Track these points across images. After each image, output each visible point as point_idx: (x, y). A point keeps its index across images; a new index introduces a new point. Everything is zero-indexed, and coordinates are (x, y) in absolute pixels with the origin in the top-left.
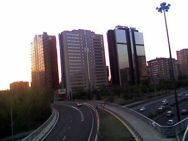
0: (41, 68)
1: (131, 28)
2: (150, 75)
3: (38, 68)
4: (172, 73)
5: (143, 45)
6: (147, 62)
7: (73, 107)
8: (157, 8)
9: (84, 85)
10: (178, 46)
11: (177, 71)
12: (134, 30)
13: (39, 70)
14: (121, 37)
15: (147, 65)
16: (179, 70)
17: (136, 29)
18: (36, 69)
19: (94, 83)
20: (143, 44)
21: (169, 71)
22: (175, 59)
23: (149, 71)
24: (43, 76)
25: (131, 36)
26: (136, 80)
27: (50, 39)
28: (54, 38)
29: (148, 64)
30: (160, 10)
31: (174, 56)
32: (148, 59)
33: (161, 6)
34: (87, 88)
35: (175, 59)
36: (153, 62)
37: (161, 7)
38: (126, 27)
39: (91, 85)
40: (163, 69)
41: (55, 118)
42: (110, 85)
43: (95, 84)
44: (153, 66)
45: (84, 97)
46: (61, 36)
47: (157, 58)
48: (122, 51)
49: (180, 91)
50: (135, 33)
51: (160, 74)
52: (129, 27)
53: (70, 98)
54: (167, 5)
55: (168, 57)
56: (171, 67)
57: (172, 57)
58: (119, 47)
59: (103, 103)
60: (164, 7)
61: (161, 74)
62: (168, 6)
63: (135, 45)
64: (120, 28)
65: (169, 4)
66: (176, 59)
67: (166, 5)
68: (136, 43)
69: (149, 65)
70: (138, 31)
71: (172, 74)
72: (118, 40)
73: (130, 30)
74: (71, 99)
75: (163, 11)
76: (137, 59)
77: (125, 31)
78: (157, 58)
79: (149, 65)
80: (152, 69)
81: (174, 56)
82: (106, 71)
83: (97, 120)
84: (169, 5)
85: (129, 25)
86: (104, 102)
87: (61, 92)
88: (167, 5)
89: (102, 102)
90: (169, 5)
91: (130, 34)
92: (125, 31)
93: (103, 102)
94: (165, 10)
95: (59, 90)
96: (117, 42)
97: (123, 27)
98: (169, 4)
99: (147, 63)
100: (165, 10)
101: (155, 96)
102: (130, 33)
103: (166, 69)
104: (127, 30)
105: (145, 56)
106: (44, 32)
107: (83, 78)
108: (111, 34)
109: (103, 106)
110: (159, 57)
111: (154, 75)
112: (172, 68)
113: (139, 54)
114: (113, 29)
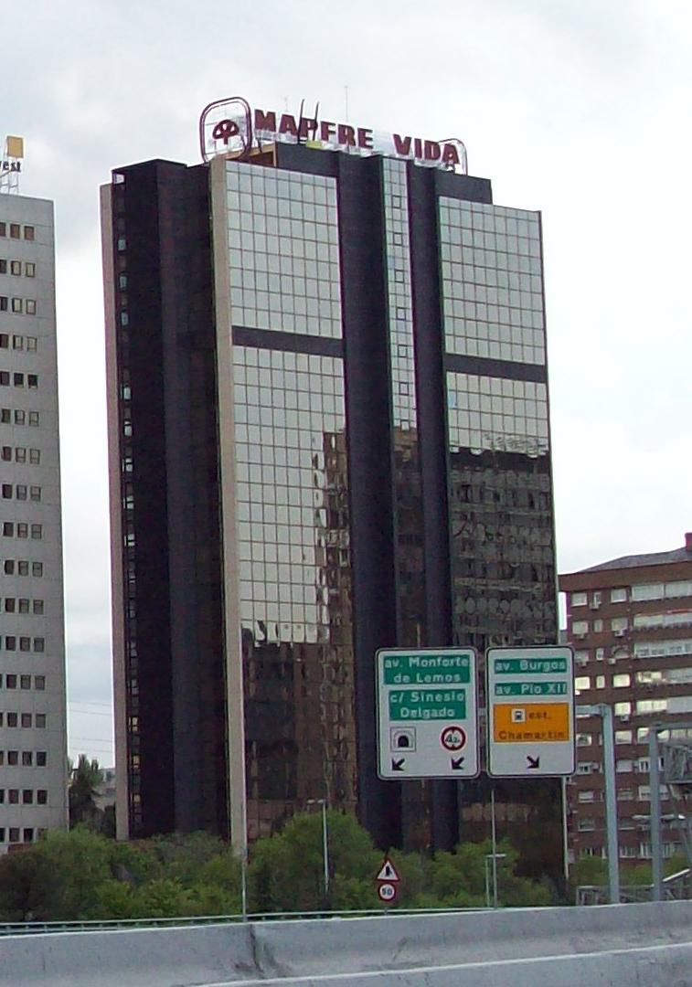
1: (402, 145)
4: (507, 667)
5: (538, 374)
6: (576, 583)
12: (438, 180)
14: (275, 257)
17: (474, 165)
25: (398, 256)
36: (641, 594)
38: (346, 133)
44: (640, 651)
48: (278, 428)
50: (451, 211)
52: (382, 143)
58: (244, 376)
64: (289, 147)
68: (451, 346)
69: (581, 628)
70: (479, 190)
72: (244, 295)
73: (395, 187)
77: (333, 181)
79: (581, 628)
80: (622, 681)
83: (289, 983)
85: (389, 115)
92: (333, 181)
93: (388, 872)
97: (314, 140)
102: (397, 220)
104: (357, 177)
108: (160, 219)
114: (193, 159)
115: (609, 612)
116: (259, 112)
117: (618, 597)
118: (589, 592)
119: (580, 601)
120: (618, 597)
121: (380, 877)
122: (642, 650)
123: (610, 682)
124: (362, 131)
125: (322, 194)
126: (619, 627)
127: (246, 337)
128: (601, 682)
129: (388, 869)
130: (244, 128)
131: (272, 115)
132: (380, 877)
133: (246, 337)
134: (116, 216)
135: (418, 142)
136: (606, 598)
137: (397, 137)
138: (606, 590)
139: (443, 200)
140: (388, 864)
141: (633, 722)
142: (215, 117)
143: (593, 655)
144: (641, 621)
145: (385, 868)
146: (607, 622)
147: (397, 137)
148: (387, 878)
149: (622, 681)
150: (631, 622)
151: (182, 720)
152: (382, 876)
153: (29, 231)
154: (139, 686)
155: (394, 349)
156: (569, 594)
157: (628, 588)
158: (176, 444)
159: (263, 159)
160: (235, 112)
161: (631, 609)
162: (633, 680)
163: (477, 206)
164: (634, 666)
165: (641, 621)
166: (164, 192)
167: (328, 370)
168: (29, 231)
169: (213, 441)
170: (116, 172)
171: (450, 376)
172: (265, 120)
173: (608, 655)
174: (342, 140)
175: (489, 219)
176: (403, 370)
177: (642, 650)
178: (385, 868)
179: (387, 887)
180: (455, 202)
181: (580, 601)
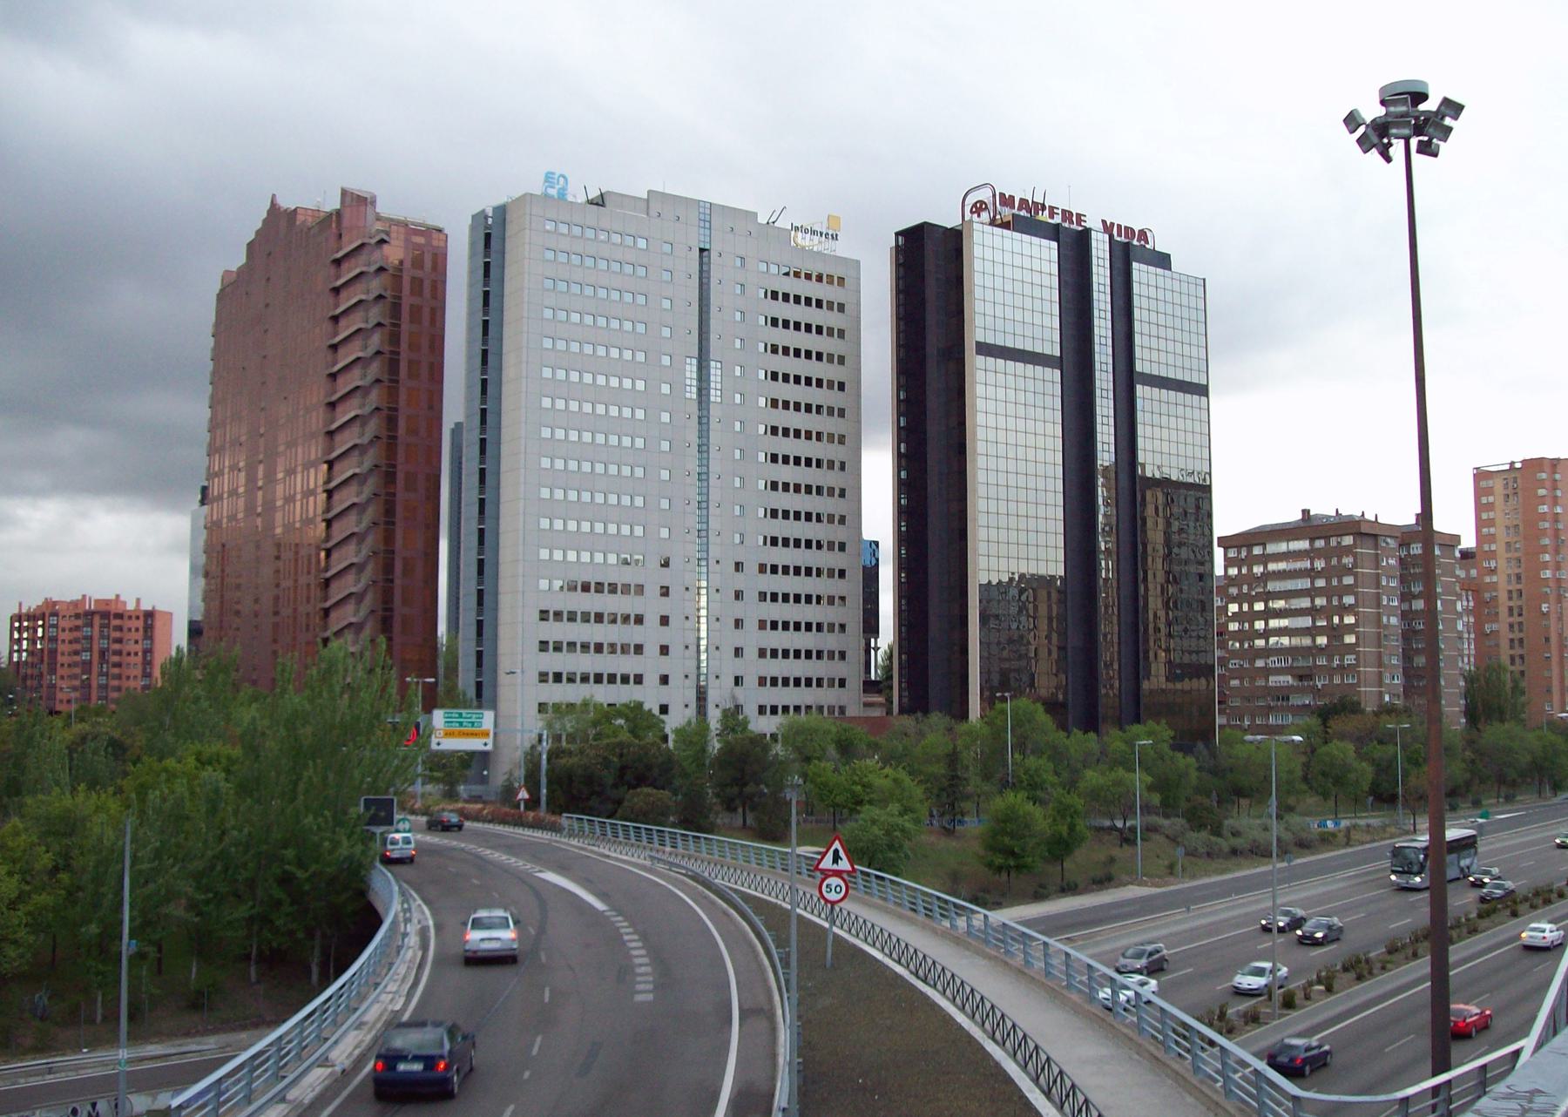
0: (290, 499)
1: (1107, 228)
2: (1235, 683)
3: (270, 507)
5: (1202, 390)
6: (1226, 542)
7: (551, 877)
8: (1352, 121)
9: (649, 697)
10: (1486, 431)
11: (1469, 648)
12: (1130, 251)
13: (270, 526)
14: (1011, 287)
15: (1219, 570)
16: (1481, 636)
18: (250, 509)
19: (738, 681)
20: (1195, 379)
21: (1394, 621)
22: (1456, 539)
23: (1234, 626)
24: (303, 580)
26: (1111, 686)
27: (394, 253)
28: (427, 249)
29: (1229, 562)
30: (1376, 137)
31: (1456, 517)
32: (1228, 519)
33: (1383, 103)
34: (672, 722)
35: (1456, 539)
36: (1272, 548)
37: (1381, 111)
38: (1067, 215)
39: (713, 696)
40: (1349, 620)
41: (411, 950)
42: (877, 713)
43: (751, 697)
44: (1271, 586)
45: (644, 795)
46: (491, 236)
47: (1305, 512)
48: (1013, 431)
49: (1313, 569)
50: (1141, 272)
51: (1322, 661)
53: (523, 794)
54: (1430, 105)
55: (1403, 513)
56: (1419, 605)
57: (1440, 524)
59: (838, 873)
60: (1409, 122)
61: (1330, 660)
62: (1439, 115)
63: (1127, 379)
64: (1024, 218)
65: (1446, 102)
66: (1468, 541)
67: (1422, 107)
68: (1138, 368)
69: (1233, 571)
70: (1163, 261)
71: (1421, 677)
73: (1100, 248)
74: (533, 803)
75: (1397, 149)
76: (1134, 517)
77: (1054, 245)
78: (1305, 512)
79: (1233, 571)
80: (1259, 606)
81: (1456, 517)
82: (852, 587)
84: (1453, 108)
86: (844, 864)
87: (448, 734)
88: (1430, 105)
89: (827, 863)
90: (1453, 108)
91: (1098, 270)
93: (836, 858)
94: (1414, 142)
95: (439, 717)
96: (980, 336)
97: (1044, 216)
98: (1446, 102)
99: (1219, 553)
100: (1414, 142)
101: (1266, 854)
103: (1378, 597)
104: (1074, 246)
105: (1207, 489)
106: (344, 193)
107: (651, 635)
109: (833, 896)
110: (1323, 508)
111: (1274, 680)
112: (1431, 614)
113: (1159, 454)
114: (950, 220)
115: (1251, 560)
116: (1002, 195)
117: (1257, 551)
118: (1239, 547)
119: (1232, 554)
120: (1257, 551)
121: (822, 866)
122: (1272, 586)
123: (1251, 607)
124: (1079, 216)
125: (1046, 253)
126: (1258, 570)
127: (985, 349)
128: (1245, 607)
129: (836, 851)
130: (991, 207)
131: (1012, 198)
132: (822, 866)
133: (985, 349)
134: (898, 265)
135: (1119, 226)
136: (1250, 551)
137: (1104, 222)
138: (1250, 547)
139: (1135, 265)
140: (837, 845)
141: (1267, 634)
142: (971, 200)
143: (1240, 589)
144: (1272, 567)
145: (831, 852)
146: (1252, 679)
147: (1104, 222)
148: (835, 867)
149: (1259, 606)
150: (1265, 567)
151: (936, 627)
152: (827, 863)
153: (841, 280)
154: (908, 604)
155: (1097, 366)
156: (1226, 549)
157: (1264, 545)
158: (935, 430)
159: (1005, 225)
160: (985, 195)
161: (1265, 559)
162: (1314, 641)
163: (1160, 271)
164: (1267, 597)
165: (1272, 567)
166: (929, 246)
167: (1045, 255)
168: (841, 280)
169: (962, 424)
170: (897, 234)
171: (1139, 388)
172: (1007, 201)
173: (1250, 589)
174: (1064, 220)
175: (1168, 281)
176: (1104, 380)
177: (1272, 586)
178: (831, 852)
179: (834, 881)
180: (1144, 267)
181: (1232, 554)
